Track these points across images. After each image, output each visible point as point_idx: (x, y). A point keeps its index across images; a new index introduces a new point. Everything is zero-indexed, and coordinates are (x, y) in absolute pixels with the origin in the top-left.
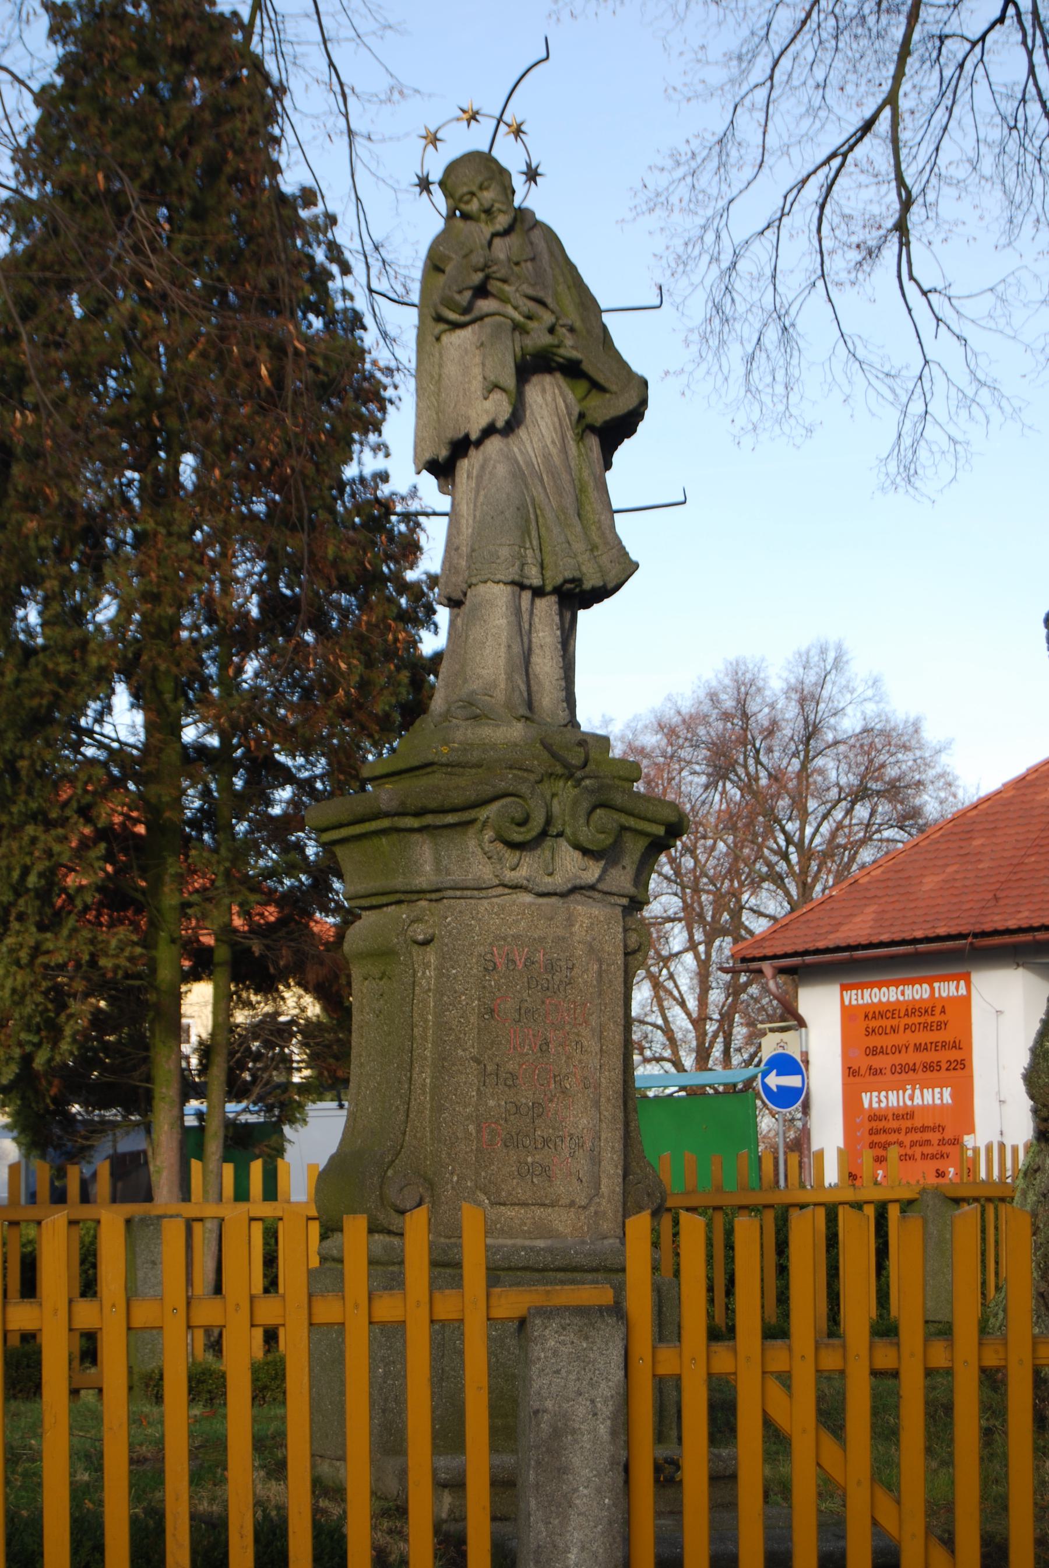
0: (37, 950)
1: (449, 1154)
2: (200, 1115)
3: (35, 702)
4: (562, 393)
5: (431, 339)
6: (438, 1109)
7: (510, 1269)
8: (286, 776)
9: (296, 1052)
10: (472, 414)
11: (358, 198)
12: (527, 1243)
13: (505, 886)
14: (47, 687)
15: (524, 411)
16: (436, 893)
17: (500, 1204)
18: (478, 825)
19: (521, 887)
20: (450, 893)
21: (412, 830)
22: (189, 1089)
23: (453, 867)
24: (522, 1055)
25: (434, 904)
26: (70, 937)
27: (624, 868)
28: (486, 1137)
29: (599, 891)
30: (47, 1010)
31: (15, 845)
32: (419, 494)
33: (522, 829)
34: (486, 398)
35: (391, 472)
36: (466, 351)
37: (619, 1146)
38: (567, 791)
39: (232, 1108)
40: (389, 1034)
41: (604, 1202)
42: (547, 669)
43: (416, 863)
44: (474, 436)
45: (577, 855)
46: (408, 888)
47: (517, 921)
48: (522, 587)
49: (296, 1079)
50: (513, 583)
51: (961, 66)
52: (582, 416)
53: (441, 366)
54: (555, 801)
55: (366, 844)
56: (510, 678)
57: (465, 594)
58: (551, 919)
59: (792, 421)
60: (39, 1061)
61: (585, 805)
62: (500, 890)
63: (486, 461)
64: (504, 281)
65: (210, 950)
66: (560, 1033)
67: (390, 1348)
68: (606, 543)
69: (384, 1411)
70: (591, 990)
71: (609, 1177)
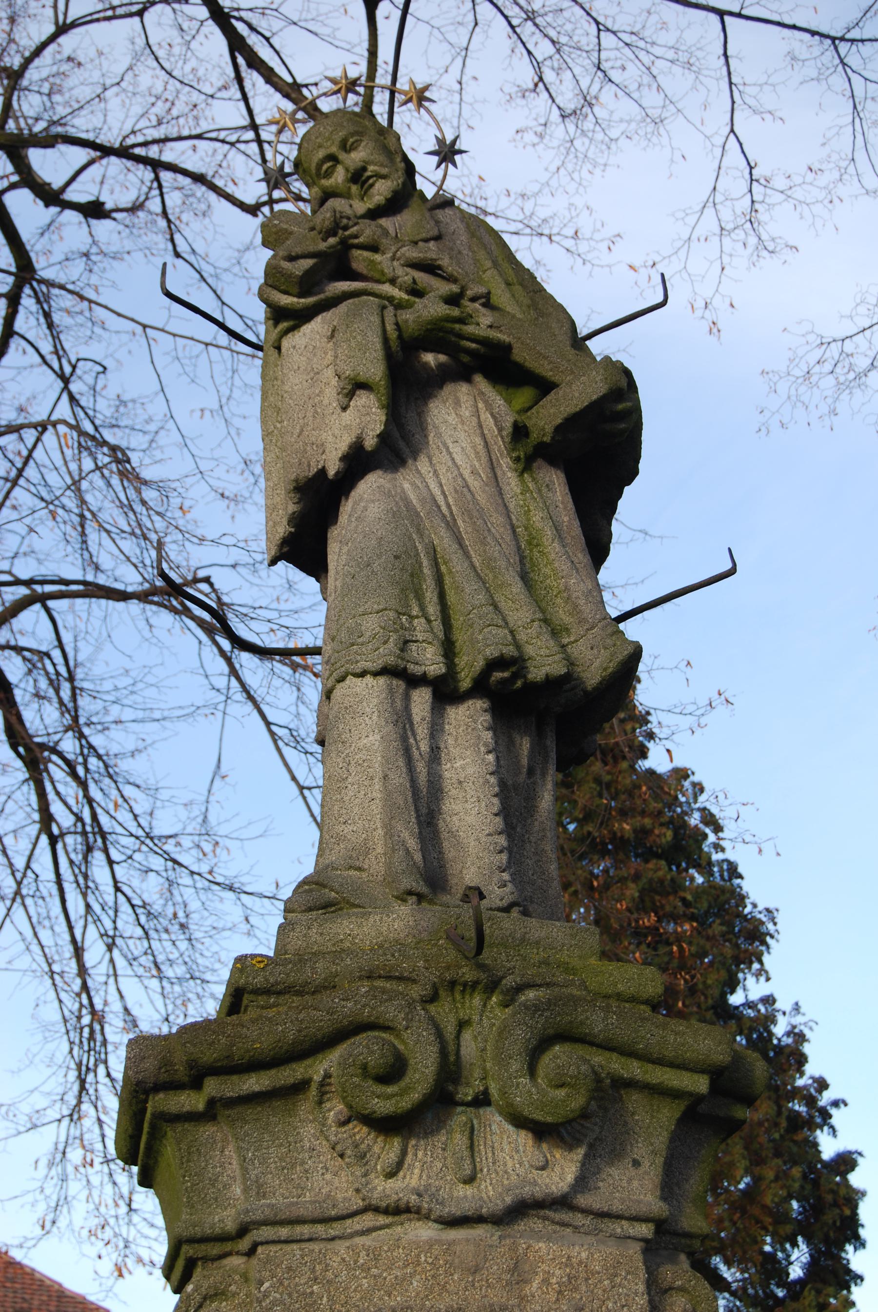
4: (489, 407)
10: (327, 437)
13: (377, 1210)
18: (313, 1091)
19: (408, 1210)
20: (266, 1233)
21: (192, 1117)
23: (272, 1181)
29: (586, 1212)
32: (802, 1010)
33: (390, 1090)
34: (344, 409)
35: (776, 996)
42: (471, 819)
43: (213, 1182)
45: (524, 1138)
46: (198, 1232)
48: (414, 681)
50: (384, 671)
52: (519, 432)
54: (467, 1036)
56: (389, 833)
58: (476, 1270)
61: (521, 1036)
62: (368, 1220)
64: (374, 248)
68: (582, 621)
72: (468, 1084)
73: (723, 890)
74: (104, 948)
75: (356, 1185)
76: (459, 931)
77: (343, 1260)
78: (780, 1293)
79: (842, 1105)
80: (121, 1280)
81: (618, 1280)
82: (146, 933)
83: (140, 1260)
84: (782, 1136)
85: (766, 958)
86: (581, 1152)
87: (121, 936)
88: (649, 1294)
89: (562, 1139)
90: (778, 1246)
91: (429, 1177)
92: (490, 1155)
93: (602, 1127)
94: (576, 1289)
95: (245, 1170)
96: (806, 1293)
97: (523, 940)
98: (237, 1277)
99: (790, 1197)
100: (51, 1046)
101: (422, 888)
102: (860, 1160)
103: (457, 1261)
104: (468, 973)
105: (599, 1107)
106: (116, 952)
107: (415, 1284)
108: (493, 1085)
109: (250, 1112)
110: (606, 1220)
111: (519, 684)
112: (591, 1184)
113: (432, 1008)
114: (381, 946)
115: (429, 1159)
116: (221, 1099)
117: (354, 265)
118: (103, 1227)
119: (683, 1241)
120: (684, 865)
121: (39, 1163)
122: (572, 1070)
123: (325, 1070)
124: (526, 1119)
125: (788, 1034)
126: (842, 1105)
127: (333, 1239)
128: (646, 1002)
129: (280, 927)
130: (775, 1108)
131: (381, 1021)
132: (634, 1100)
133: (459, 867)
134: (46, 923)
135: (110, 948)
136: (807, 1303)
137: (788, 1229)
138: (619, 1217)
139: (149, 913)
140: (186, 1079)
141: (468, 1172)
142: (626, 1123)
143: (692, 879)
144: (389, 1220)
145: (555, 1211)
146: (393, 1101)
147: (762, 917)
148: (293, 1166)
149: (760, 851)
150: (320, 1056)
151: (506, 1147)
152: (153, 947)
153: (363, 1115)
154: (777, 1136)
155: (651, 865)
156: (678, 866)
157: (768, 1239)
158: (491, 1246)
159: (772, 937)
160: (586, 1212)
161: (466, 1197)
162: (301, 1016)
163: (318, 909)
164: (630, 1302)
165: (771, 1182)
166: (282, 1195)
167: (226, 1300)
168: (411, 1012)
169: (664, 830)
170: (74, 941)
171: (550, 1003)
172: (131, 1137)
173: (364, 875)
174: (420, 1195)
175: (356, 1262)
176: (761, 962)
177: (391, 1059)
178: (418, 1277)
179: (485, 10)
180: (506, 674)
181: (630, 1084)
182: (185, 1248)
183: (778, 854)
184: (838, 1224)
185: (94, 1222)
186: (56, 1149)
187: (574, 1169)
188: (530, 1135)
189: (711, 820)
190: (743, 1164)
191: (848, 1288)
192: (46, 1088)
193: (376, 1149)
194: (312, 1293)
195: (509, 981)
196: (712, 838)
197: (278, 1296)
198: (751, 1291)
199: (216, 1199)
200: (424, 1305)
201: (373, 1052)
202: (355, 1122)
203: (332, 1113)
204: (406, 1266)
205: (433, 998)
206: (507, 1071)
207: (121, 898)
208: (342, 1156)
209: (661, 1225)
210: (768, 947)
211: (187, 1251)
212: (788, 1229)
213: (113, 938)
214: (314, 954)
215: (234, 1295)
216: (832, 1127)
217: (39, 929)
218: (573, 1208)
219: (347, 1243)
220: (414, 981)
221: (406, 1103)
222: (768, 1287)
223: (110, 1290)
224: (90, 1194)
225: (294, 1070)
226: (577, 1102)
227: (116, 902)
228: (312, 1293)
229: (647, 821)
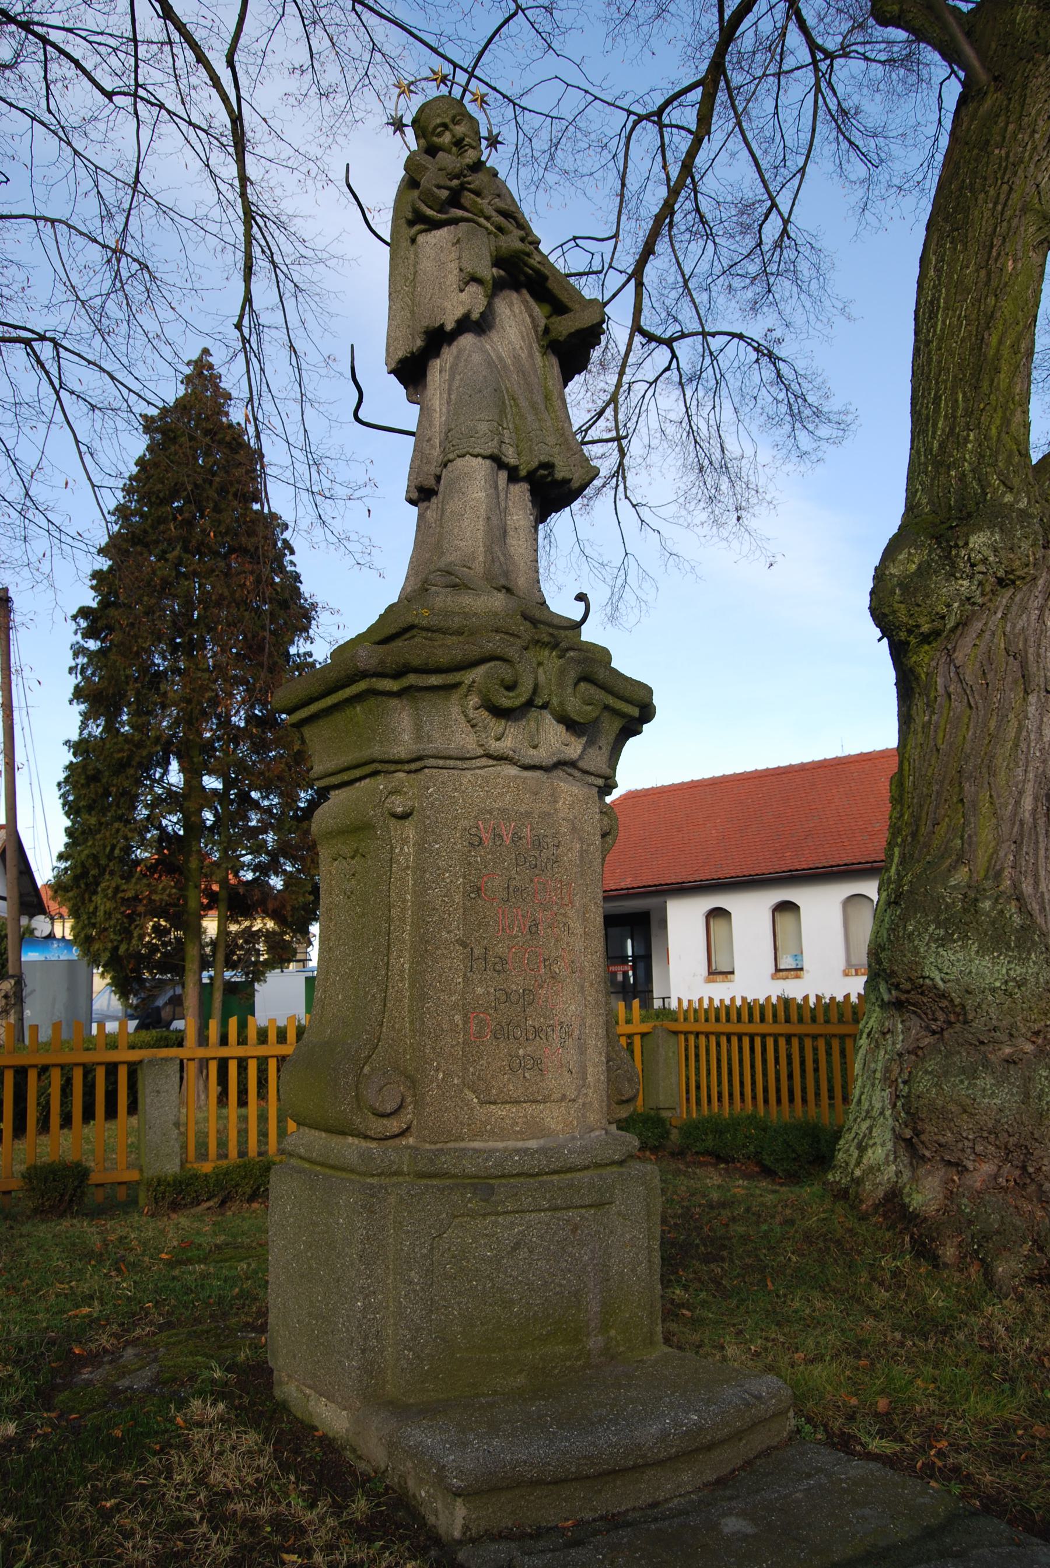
0: (117, 890)
1: (434, 1048)
2: (211, 978)
3: (120, 755)
5: (405, 243)
6: (420, 997)
8: (256, 805)
9: (261, 947)
10: (448, 305)
11: (305, 431)
12: (520, 1144)
13: (489, 756)
14: (126, 747)
15: (494, 319)
16: (415, 763)
17: (490, 1103)
18: (463, 689)
19: (506, 759)
20: (432, 762)
21: (390, 694)
22: (205, 964)
23: (436, 735)
25: (413, 776)
26: (136, 883)
27: (600, 748)
28: (474, 1028)
29: (580, 770)
30: (123, 923)
31: (108, 834)
33: (511, 694)
34: (462, 291)
36: (442, 248)
38: (552, 662)
39: (228, 974)
40: (363, 915)
42: (522, 551)
43: (393, 731)
44: (449, 326)
45: (561, 728)
46: (386, 757)
49: (262, 959)
51: (643, 397)
52: (547, 330)
53: (416, 264)
55: (339, 718)
57: (438, 478)
59: (551, 582)
60: (122, 950)
62: (484, 761)
63: (460, 352)
64: (478, 194)
65: (216, 893)
67: (369, 1277)
69: (363, 1351)
70: (575, 870)
71: (595, 1066)
86: (585, 739)
89: (575, 732)
109: (428, 695)
111: (549, 479)
117: (463, 201)
138: (592, 774)
144: (495, 763)
179: (291, 8)
180: (546, 472)
193: (491, 725)
195: (563, 645)
215: (406, 793)
220: (519, 637)
221: (518, 702)
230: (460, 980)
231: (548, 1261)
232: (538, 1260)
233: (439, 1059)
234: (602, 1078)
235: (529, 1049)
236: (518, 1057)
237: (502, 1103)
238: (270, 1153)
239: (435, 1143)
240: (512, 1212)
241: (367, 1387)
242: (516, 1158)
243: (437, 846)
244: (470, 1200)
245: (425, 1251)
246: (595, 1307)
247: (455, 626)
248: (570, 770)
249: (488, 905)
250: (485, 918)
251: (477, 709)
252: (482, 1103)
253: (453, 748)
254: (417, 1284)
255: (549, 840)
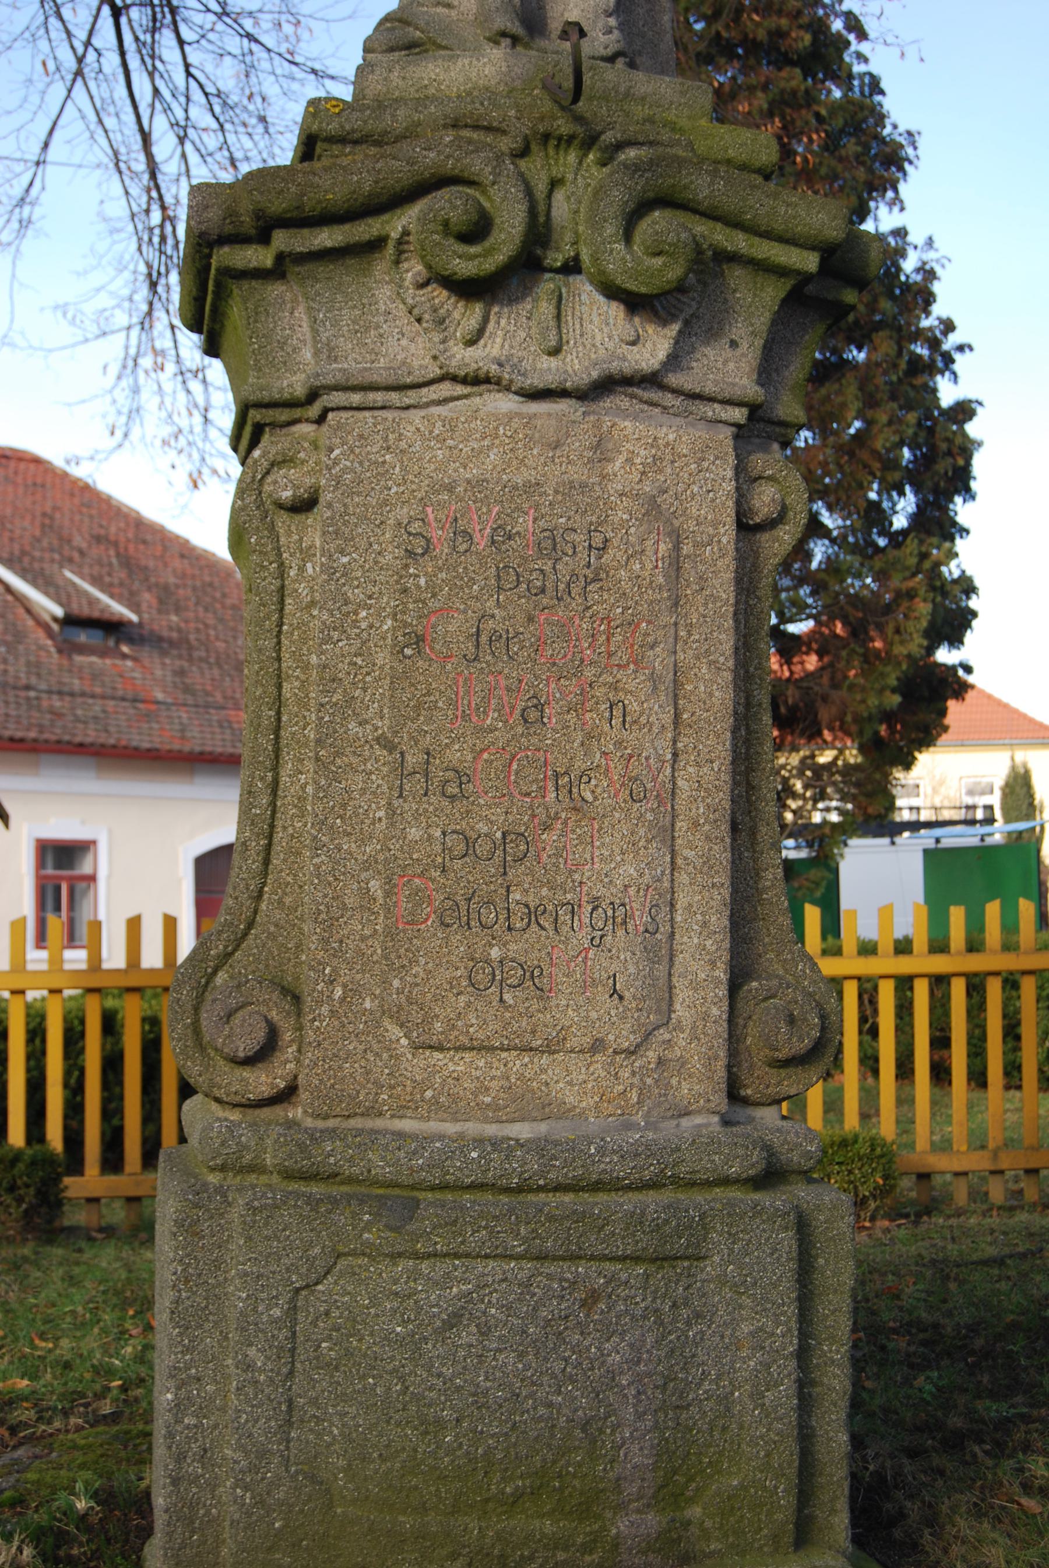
7: (444, 1187)
12: (491, 1130)
13: (454, 379)
17: (431, 1047)
18: (390, 249)
19: (487, 380)
23: (345, 345)
24: (481, 731)
27: (734, 344)
29: (676, 392)
32: (936, 245)
33: (473, 250)
35: (909, 229)
37: (719, 921)
41: (682, 1039)
43: (282, 345)
45: (616, 310)
46: (266, 396)
47: (478, 453)
54: (559, 196)
61: (618, 197)
62: (446, 389)
66: (572, 685)
67: (187, 1350)
72: (558, 249)
73: (862, 107)
74: (175, 140)
75: (434, 352)
76: (557, 80)
77: (418, 430)
78: (882, 542)
79: (967, 350)
80: (196, 492)
81: (705, 464)
82: (222, 126)
83: (215, 472)
84: (900, 380)
85: (902, 187)
86: (676, 327)
87: (194, 128)
88: (737, 480)
89: (656, 313)
90: (885, 496)
91: (512, 347)
92: (578, 326)
93: (699, 303)
94: (661, 471)
95: (315, 332)
96: (909, 541)
97: (627, 94)
98: (306, 445)
99: (901, 444)
100: (119, 248)
101: (518, 29)
102: (979, 410)
103: (537, 435)
104: (563, 126)
105: (699, 281)
106: (189, 147)
107: (492, 457)
108: (585, 251)
109: (321, 269)
110: (697, 402)
112: (684, 363)
113: (523, 164)
114: (469, 93)
115: (513, 328)
116: (290, 254)
118: (176, 437)
119: (777, 429)
120: (821, 75)
121: (109, 369)
122: (672, 237)
123: (404, 227)
124: (619, 288)
125: (918, 270)
126: (967, 350)
127: (408, 408)
128: (759, 171)
129: (358, 68)
130: (896, 348)
131: (466, 174)
132: (737, 276)
133: (561, 8)
134: (111, 109)
135: (182, 140)
136: (908, 551)
137: (897, 476)
138: (711, 399)
139: (225, 103)
140: (253, 232)
141: (553, 343)
142: (726, 301)
143: (829, 92)
144: (467, 390)
145: (644, 389)
146: (476, 262)
147: (902, 140)
148: (367, 329)
149: (903, 54)
150: (399, 211)
151: (596, 319)
152: (229, 142)
153: (442, 276)
154: (894, 378)
155: (784, 74)
156: (814, 78)
157: (875, 486)
158: (574, 422)
159: (911, 163)
160: (676, 392)
161: (549, 369)
162: (378, 166)
163: (401, 50)
164: (716, 488)
165: (884, 426)
166: (355, 360)
167: (294, 467)
168: (498, 165)
169: (802, 33)
170: (141, 129)
171: (652, 164)
172: (196, 299)
173: (453, 13)
174: (501, 365)
175: (431, 432)
176: (896, 190)
177: (475, 217)
178: (495, 450)
181: (733, 258)
182: (252, 412)
183: (922, 60)
184: (950, 474)
185: (167, 431)
186: (127, 354)
187: (667, 346)
188: (622, 307)
189: (854, 25)
190: (854, 406)
191: (952, 540)
192: (112, 287)
193: (456, 315)
194: (384, 462)
195: (609, 137)
196: (855, 46)
197: (348, 464)
198: (851, 539)
199: (285, 363)
200: (500, 478)
201: (454, 207)
202: (435, 285)
203: (410, 274)
204: (483, 439)
205: (524, 152)
206: (601, 235)
207: (193, 83)
208: (419, 320)
209: (754, 410)
210: (905, 174)
211: (254, 415)
212: (897, 476)
213: (185, 128)
214: (396, 100)
215: (303, 462)
216: (954, 374)
217: (102, 115)
218: (663, 387)
219: (423, 413)
220: (504, 132)
221: (490, 265)
222: (870, 536)
223: (185, 506)
224: (162, 402)
225: (369, 226)
226: (674, 273)
227: (187, 89)
228: (384, 462)
229: (784, 22)
230: (381, 814)
231: (521, 1355)
232: (499, 1350)
233: (335, 962)
234: (715, 1011)
235: (512, 947)
236: (488, 961)
237: (457, 1049)
238: (919, 1147)
239: (326, 1117)
240: (446, 1255)
241: (183, 1546)
242: (474, 1155)
243: (345, 560)
244: (367, 1228)
245: (277, 1312)
246: (638, 1455)
247: (399, 127)
248: (654, 395)
249: (435, 668)
250: (429, 694)
251: (422, 286)
252: (417, 1047)
253: (380, 370)
254: (261, 1370)
255: (577, 538)
